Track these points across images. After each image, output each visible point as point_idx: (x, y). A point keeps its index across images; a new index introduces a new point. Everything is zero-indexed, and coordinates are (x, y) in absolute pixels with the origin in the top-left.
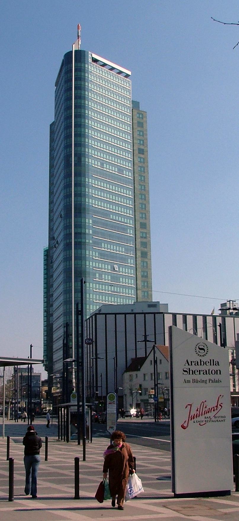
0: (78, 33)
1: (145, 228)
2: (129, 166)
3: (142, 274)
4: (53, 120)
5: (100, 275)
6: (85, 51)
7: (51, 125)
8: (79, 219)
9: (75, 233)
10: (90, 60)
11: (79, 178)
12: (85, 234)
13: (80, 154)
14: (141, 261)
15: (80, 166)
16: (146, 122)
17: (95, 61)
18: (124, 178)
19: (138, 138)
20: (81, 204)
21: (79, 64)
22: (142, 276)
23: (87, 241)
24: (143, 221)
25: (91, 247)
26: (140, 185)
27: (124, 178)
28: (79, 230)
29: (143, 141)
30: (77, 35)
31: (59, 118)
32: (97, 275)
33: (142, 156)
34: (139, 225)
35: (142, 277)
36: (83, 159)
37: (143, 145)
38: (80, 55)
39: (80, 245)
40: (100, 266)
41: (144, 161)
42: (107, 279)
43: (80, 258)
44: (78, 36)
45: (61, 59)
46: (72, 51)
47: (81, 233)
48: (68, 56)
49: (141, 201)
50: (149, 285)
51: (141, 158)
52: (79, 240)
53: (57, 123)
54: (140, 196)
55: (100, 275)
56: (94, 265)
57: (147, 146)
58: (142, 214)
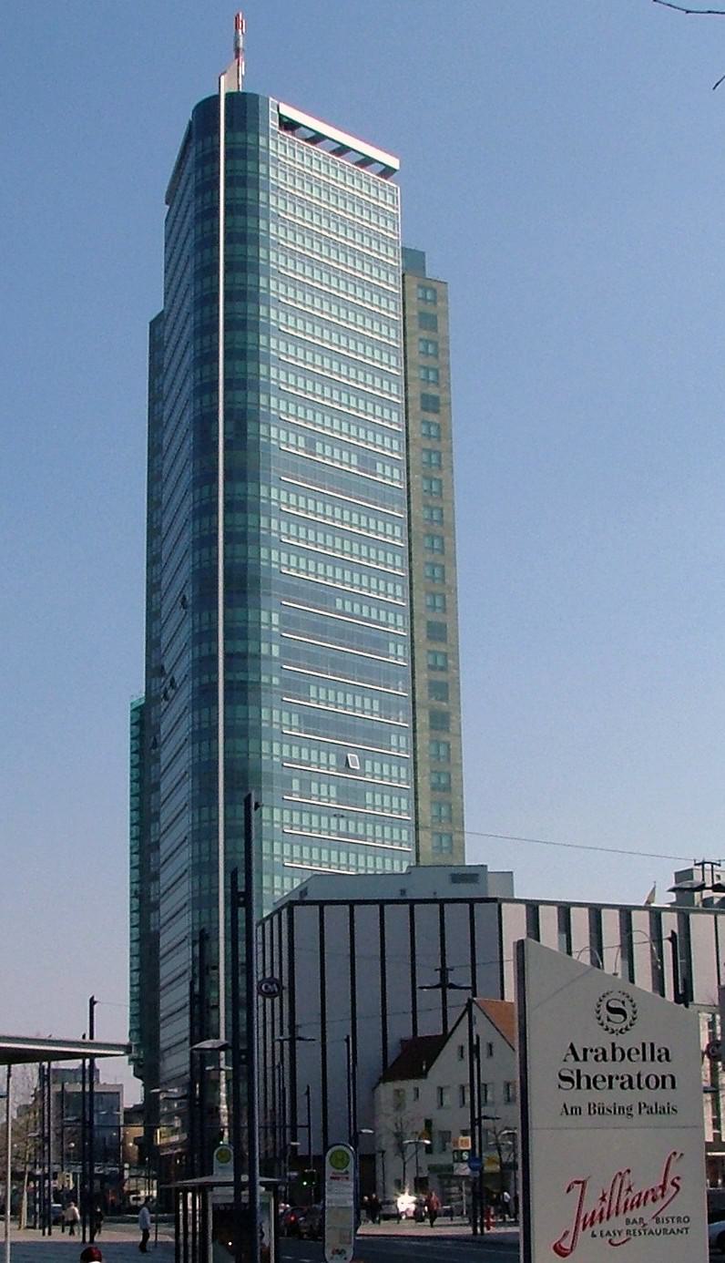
1: (443, 639)
2: (394, 449)
6: (256, 97)
8: (239, 612)
9: (227, 655)
10: (274, 124)
12: (258, 656)
13: (244, 413)
14: (431, 741)
17: (289, 125)
19: (421, 362)
20: (244, 567)
21: (239, 137)
22: (434, 788)
23: (264, 679)
26: (427, 506)
29: (436, 371)
32: (295, 783)
33: (432, 418)
35: (433, 789)
36: (251, 427)
38: (243, 108)
39: (241, 692)
40: (305, 757)
42: (326, 796)
43: (242, 731)
45: (183, 119)
46: (217, 97)
48: (207, 109)
49: (429, 558)
51: (429, 424)
54: (427, 542)
56: (286, 754)
57: (448, 388)
58: (433, 595)
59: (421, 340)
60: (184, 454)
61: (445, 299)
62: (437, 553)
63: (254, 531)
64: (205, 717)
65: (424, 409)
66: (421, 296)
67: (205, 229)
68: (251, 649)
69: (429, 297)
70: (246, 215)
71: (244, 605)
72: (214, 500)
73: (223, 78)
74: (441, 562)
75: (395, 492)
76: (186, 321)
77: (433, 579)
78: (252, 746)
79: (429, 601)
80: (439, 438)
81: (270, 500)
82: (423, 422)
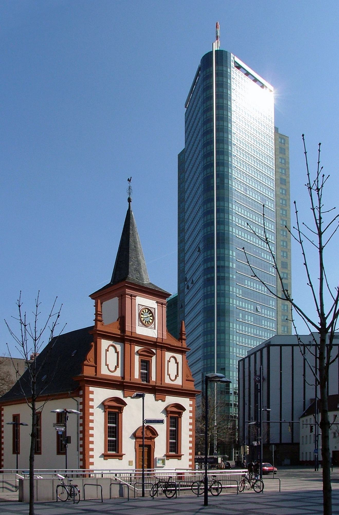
0: (217, 34)
1: (286, 268)
2: (272, 196)
3: (283, 318)
4: (182, 146)
5: (244, 316)
6: (227, 52)
7: (180, 156)
8: (222, 251)
9: (217, 267)
10: (233, 64)
11: (222, 203)
12: (229, 267)
13: (223, 175)
14: (282, 304)
15: (223, 188)
16: (288, 149)
17: (239, 67)
18: (240, 241)
19: (280, 166)
20: (224, 234)
21: (220, 68)
22: (283, 321)
23: (231, 276)
24: (284, 260)
25: (235, 283)
26: (282, 219)
27: (240, 241)
28: (222, 263)
29: (285, 170)
30: (215, 36)
31: (191, 145)
32: (241, 315)
33: (283, 187)
34: (280, 264)
35: (282, 321)
36: (226, 181)
37: (285, 174)
38: (222, 56)
39: (223, 280)
40: (244, 306)
41: (287, 192)
42: (250, 319)
43: (223, 295)
44: (217, 37)
45: (197, 63)
46: (212, 52)
47: (224, 267)
48: (207, 59)
49: (282, 238)
50: (289, 330)
51: (282, 189)
52: (222, 275)
53: (189, 150)
54: (281, 233)
55: (244, 316)
56: (238, 304)
57: (289, 177)
58: (283, 252)
59: (280, 158)
60: (199, 192)
61: (288, 163)
62: (283, 165)
63: (227, 220)
64: (209, 338)
65: (281, 183)
66: (281, 234)
67: (208, 302)
68: (226, 264)
69: (283, 142)
70: (224, 225)
71: (224, 284)
72: (212, 365)
73: (214, 44)
74: (286, 240)
75: (272, 212)
76: (198, 111)
77: (284, 256)
78: (227, 349)
79: (280, 140)
80: (286, 194)
81: (233, 221)
82: (281, 188)
